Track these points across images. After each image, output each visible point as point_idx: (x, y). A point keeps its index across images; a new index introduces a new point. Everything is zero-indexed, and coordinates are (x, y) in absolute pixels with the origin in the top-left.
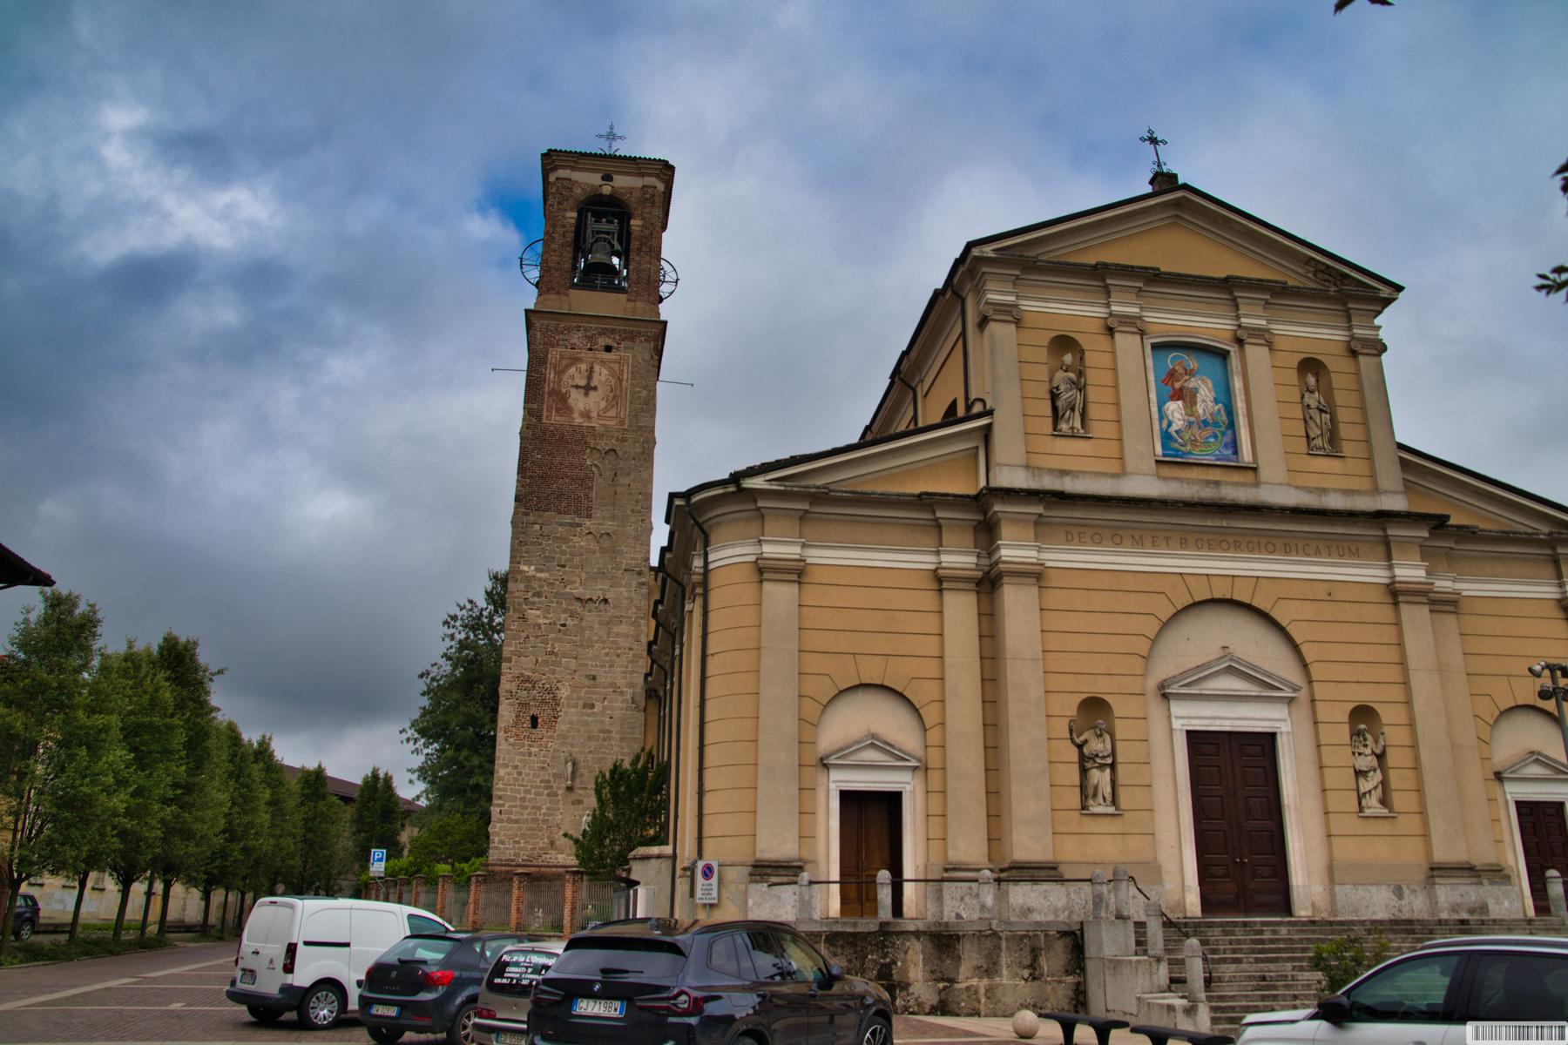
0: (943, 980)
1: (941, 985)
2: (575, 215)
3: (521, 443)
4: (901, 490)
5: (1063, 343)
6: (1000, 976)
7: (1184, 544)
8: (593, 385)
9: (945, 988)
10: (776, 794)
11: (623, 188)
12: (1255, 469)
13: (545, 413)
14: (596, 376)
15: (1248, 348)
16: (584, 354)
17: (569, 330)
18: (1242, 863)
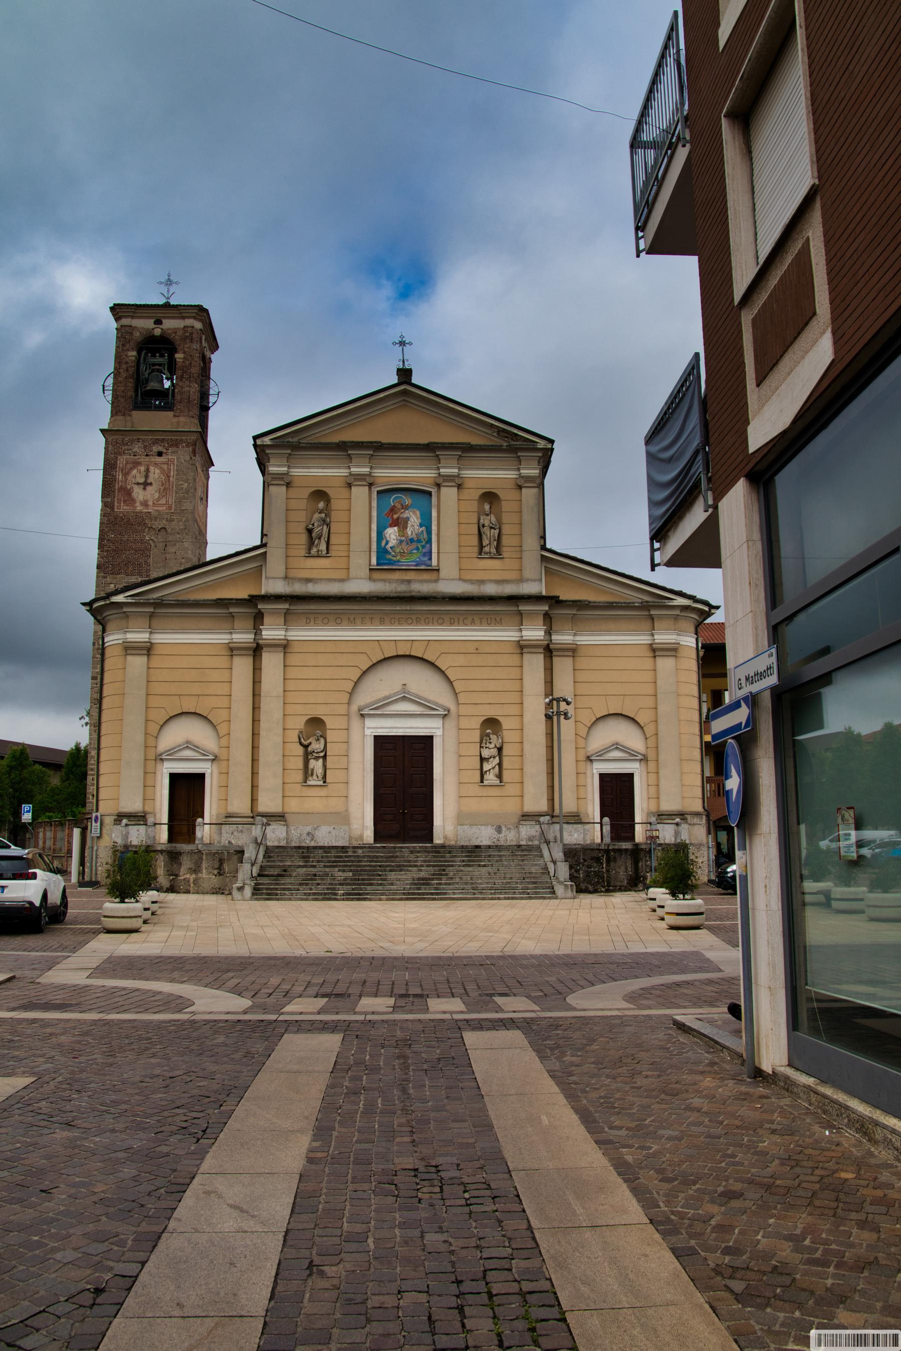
0: (172, 875)
1: (171, 878)
2: (134, 353)
3: (100, 527)
4: (206, 598)
5: (320, 495)
6: (202, 873)
7: (382, 622)
8: (149, 481)
9: (173, 879)
10: (132, 776)
11: (169, 329)
12: (438, 570)
13: (116, 504)
14: (151, 475)
15: (443, 490)
16: (144, 459)
17: (132, 441)
18: (404, 813)
